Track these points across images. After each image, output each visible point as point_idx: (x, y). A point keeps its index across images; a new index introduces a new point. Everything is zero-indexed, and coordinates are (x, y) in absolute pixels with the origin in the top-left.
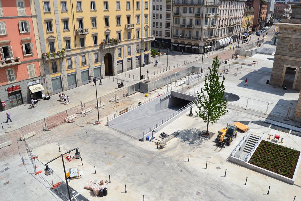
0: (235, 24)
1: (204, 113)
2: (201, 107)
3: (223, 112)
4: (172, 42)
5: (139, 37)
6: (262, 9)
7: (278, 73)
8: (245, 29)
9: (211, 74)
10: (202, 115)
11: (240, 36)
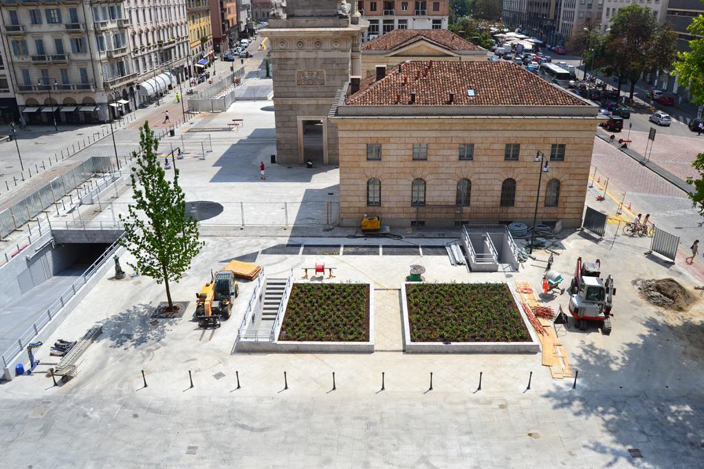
0: (172, 40)
1: (149, 262)
2: (138, 251)
3: (195, 249)
4: (18, 104)
7: (289, 136)
8: (195, 52)
9: (144, 167)
10: (148, 269)
11: (189, 67)
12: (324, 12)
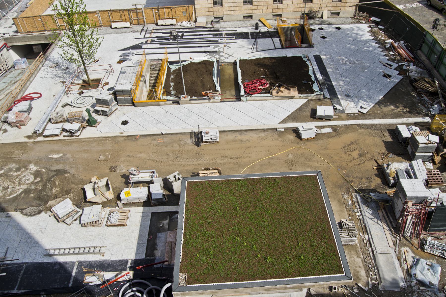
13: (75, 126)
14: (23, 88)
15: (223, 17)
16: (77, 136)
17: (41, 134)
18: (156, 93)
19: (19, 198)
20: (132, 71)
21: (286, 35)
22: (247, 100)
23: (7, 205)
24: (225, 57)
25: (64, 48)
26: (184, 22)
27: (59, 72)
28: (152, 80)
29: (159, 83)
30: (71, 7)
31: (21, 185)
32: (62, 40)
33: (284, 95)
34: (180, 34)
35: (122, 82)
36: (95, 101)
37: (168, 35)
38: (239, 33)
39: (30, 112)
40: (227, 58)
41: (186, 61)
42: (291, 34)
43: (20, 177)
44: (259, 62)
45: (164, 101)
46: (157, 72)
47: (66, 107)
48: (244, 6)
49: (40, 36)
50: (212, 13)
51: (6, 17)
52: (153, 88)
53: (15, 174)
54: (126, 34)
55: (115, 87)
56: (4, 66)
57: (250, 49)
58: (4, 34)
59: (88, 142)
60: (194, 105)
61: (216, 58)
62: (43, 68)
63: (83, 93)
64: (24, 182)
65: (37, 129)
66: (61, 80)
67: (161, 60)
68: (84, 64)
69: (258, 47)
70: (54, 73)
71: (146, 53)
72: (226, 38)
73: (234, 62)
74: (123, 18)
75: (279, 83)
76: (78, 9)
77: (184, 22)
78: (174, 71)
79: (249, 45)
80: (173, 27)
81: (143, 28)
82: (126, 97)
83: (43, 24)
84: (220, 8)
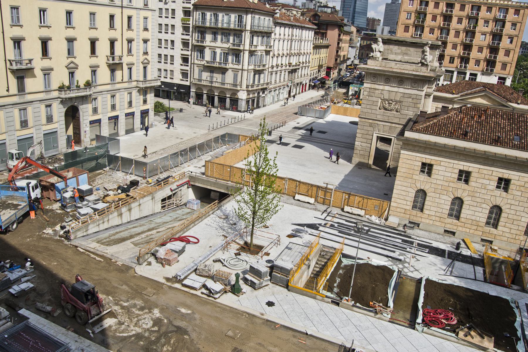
0: (298, 64)
5: (130, 78)
6: (340, 43)
8: (312, 75)
11: (306, 84)
12: (410, 59)
13: (217, 287)
14: (185, 228)
15: (419, 224)
16: (215, 298)
17: (180, 281)
18: (317, 284)
19: (128, 340)
20: (299, 250)
21: (494, 268)
22: (422, 331)
23: (113, 342)
24: (409, 270)
25: (240, 204)
26: (373, 216)
27: (225, 224)
28: (317, 267)
29: (324, 274)
30: (264, 167)
31: (136, 326)
32: (242, 195)
33: (474, 342)
34: (367, 228)
35: (284, 258)
36: (248, 267)
37: (353, 225)
38: (434, 248)
39: (180, 254)
40: (412, 272)
41: (362, 259)
42: (500, 268)
43: (140, 317)
44: (450, 289)
45: (323, 296)
46: (326, 261)
47: (218, 263)
48: (447, 219)
49: (223, 185)
50: (408, 216)
51: (200, 158)
52: (316, 276)
53: (137, 312)
54: (306, 209)
55: (274, 261)
56: (178, 201)
57: (443, 269)
58: (192, 172)
59: (224, 309)
60: (355, 313)
61: (398, 267)
62: (212, 216)
63: (240, 255)
64: (140, 325)
65: (179, 274)
66: (223, 234)
67: (335, 249)
68: (253, 226)
69: (453, 270)
70: (220, 225)
71: (321, 236)
72: (416, 249)
73: (419, 279)
74: (310, 193)
75: (471, 324)
76: (269, 172)
77: (373, 216)
78: (346, 266)
79: (443, 265)
80: (360, 218)
81: (327, 209)
82: (282, 276)
83: (230, 174)
84: (419, 214)
